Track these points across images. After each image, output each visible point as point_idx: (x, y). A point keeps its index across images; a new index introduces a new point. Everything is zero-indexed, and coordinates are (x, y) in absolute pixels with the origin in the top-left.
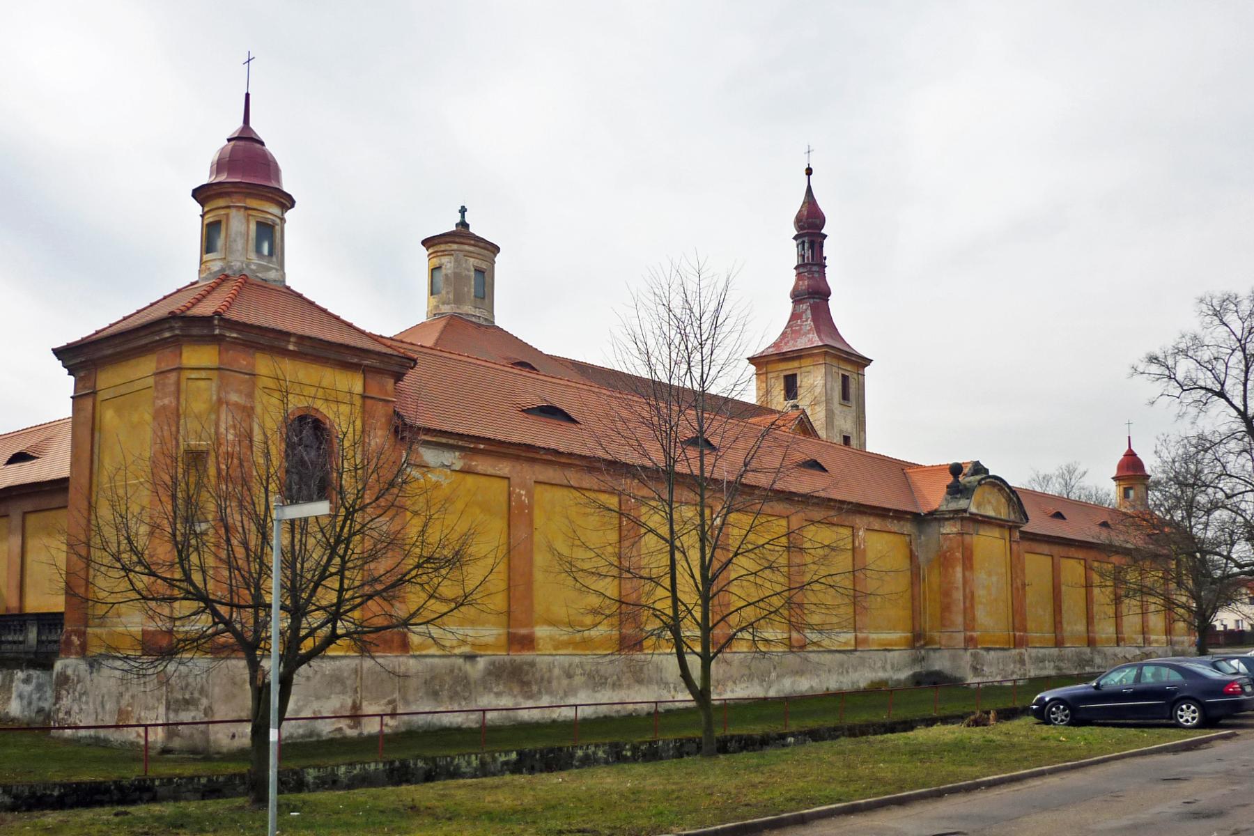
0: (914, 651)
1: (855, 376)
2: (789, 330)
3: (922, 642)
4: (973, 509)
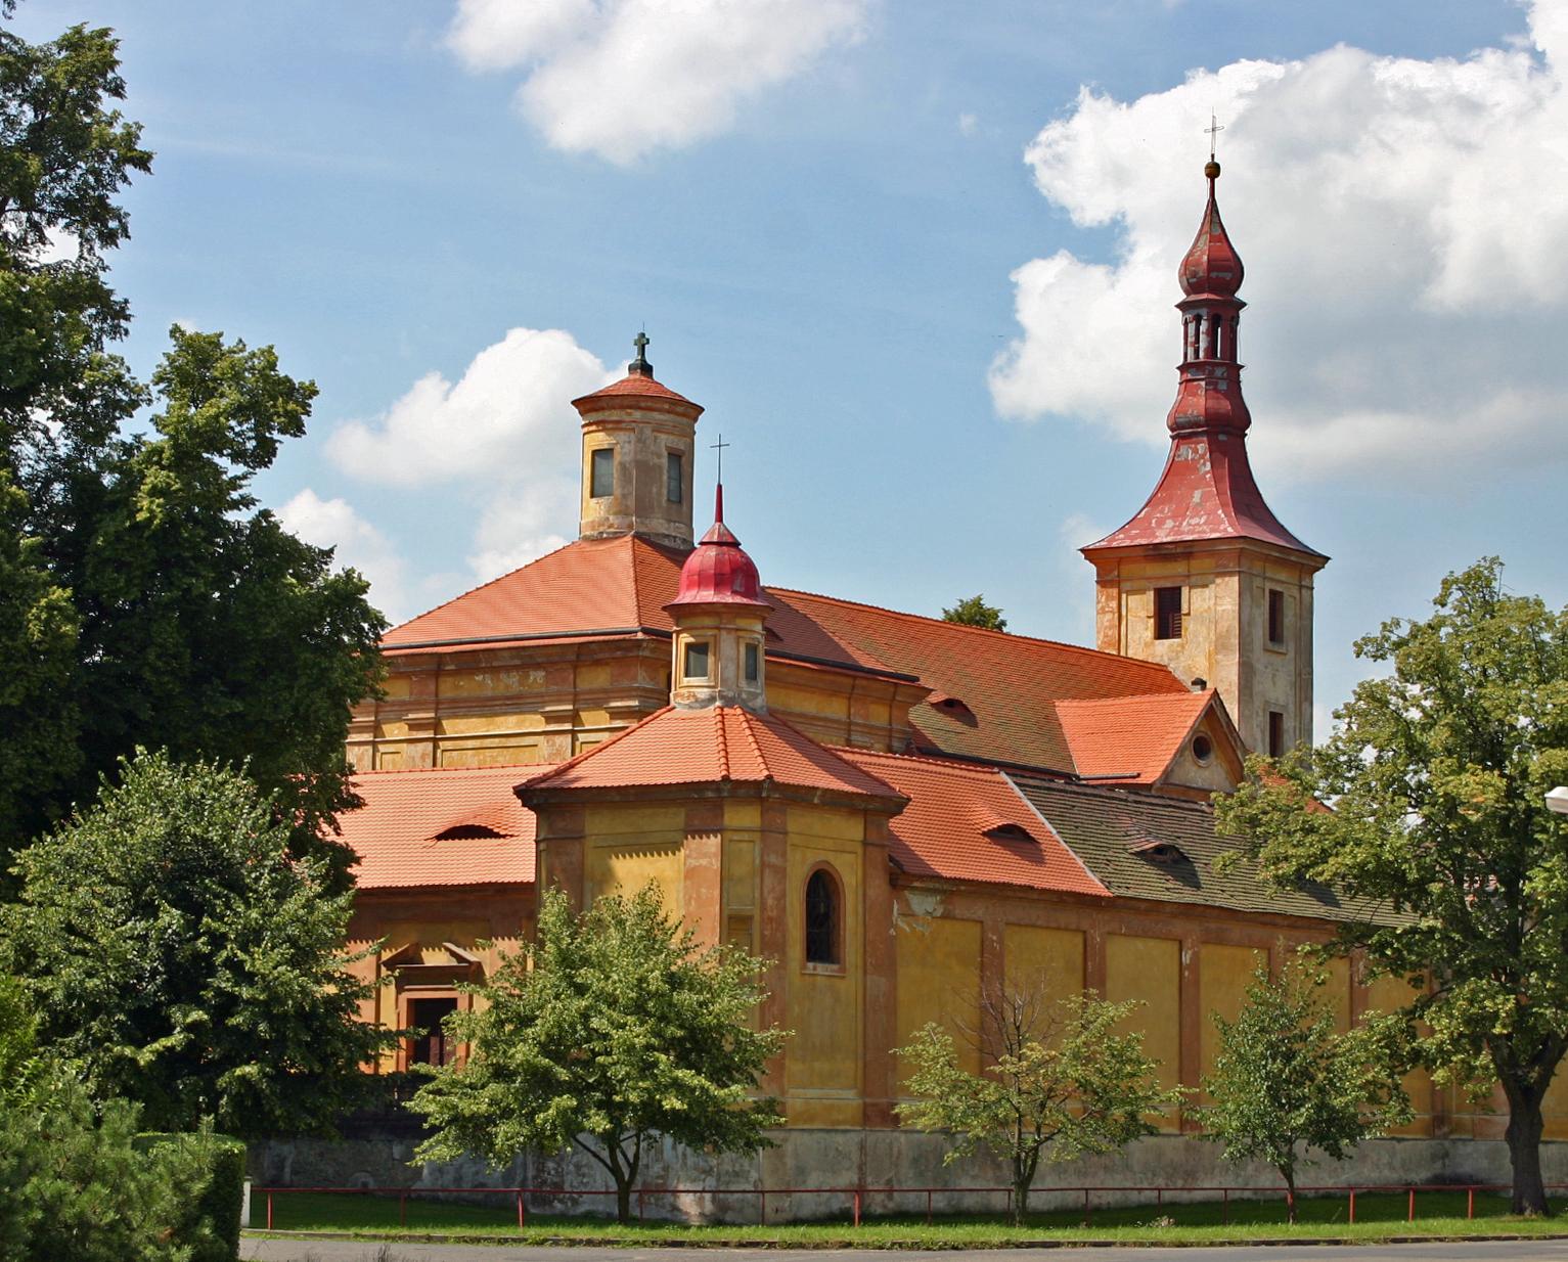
0: (1433, 1142)
1: (1295, 592)
3: (1446, 1129)
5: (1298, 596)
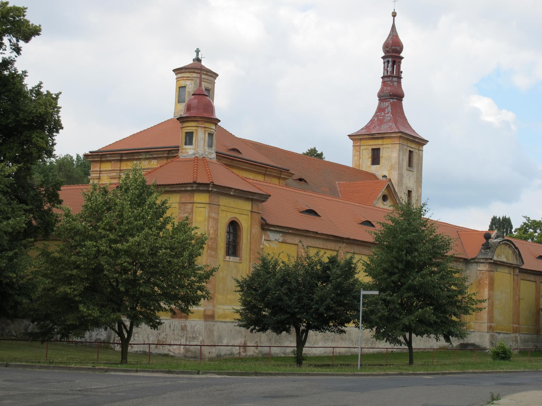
1: (417, 151)
2: (376, 119)
4: (495, 258)
5: (418, 153)
